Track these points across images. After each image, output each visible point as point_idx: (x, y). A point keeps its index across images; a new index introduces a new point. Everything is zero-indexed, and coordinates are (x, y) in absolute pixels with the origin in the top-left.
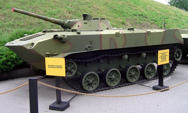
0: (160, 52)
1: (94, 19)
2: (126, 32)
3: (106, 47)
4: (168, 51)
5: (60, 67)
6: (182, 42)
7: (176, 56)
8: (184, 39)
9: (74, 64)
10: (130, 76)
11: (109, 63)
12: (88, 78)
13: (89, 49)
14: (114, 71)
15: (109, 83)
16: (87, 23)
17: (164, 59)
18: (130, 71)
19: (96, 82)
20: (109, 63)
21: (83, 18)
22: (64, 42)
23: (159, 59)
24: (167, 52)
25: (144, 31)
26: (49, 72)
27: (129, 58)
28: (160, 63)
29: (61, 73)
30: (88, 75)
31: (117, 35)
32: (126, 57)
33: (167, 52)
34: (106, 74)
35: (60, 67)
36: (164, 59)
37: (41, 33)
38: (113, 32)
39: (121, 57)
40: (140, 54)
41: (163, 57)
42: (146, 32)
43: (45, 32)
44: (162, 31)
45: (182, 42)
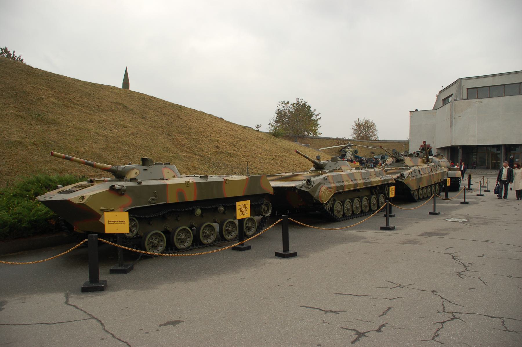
0: (238, 204)
1: (156, 164)
2: (197, 180)
3: (172, 199)
4: (248, 202)
5: (122, 222)
6: (272, 192)
7: (264, 210)
8: (275, 188)
9: (135, 221)
10: (205, 236)
11: (177, 220)
12: (152, 239)
13: (153, 202)
14: (185, 229)
15: (178, 245)
16: (389, 308)
17: (244, 212)
18: (203, 229)
19: (161, 243)
20: (177, 220)
21: (141, 162)
22: (123, 194)
23: (238, 212)
24: (247, 203)
25: (220, 179)
26: (109, 229)
27: (202, 213)
28: (239, 217)
29: (124, 228)
30: (152, 235)
31: (187, 184)
32: (199, 211)
33: (247, 203)
34: (174, 233)
35: (122, 222)
36: (244, 212)
37: (84, 183)
38: (181, 180)
39: (193, 212)
40: (216, 209)
41: (243, 210)
42: (223, 180)
43: (92, 182)
44: (244, 178)
45: (272, 192)
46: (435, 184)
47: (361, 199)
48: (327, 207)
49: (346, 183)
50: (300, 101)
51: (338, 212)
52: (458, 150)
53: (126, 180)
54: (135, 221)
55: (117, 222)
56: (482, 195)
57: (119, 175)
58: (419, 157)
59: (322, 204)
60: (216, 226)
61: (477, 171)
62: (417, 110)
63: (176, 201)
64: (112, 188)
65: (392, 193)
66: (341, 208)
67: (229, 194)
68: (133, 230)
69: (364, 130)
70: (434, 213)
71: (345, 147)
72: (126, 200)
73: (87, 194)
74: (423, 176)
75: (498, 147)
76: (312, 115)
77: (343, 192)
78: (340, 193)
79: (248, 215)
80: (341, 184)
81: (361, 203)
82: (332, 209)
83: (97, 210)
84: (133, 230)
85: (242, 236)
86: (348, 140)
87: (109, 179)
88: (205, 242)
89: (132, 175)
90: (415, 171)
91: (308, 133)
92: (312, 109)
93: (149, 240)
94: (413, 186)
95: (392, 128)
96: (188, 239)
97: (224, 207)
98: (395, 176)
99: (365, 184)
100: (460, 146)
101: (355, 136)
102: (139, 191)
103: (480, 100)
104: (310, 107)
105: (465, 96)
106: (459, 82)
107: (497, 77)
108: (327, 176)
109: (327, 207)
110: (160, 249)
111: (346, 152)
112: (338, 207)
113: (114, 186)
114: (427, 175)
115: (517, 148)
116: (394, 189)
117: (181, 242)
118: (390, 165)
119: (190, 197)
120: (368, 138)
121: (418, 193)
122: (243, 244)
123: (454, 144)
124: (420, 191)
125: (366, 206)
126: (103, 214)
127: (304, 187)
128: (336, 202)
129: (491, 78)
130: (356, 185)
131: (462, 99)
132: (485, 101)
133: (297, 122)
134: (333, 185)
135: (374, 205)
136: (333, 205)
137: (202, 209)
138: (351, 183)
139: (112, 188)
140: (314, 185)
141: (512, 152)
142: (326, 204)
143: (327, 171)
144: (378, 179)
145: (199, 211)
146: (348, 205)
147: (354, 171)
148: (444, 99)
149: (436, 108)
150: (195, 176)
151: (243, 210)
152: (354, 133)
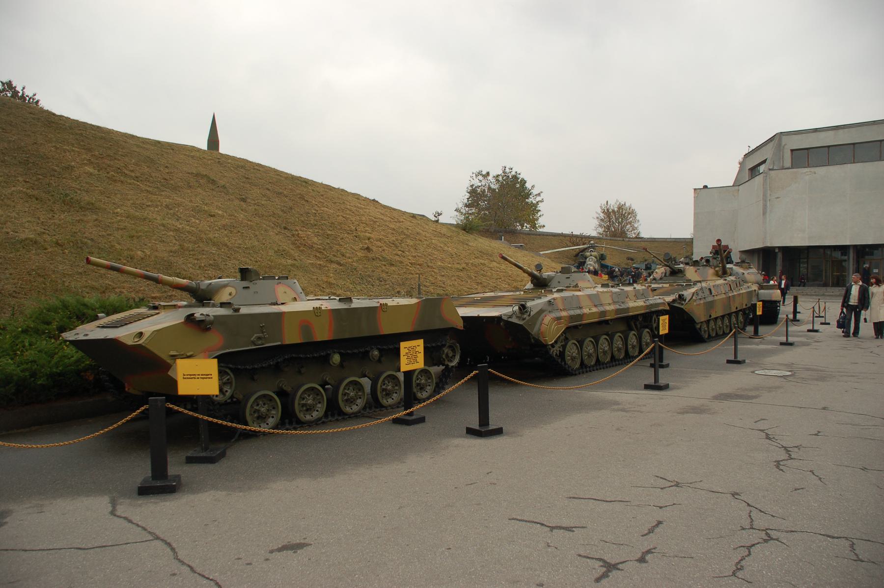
0: (403, 345)
1: (264, 278)
2: (334, 305)
3: (292, 336)
4: (421, 342)
5: (207, 376)
6: (460, 325)
7: (447, 355)
8: (465, 319)
9: (228, 374)
10: (347, 400)
11: (300, 372)
12: (258, 405)
13: (260, 342)
14: (313, 389)
15: (301, 416)
16: (660, 523)
17: (413, 359)
18: (345, 389)
19: (273, 412)
20: (300, 372)
21: (239, 275)
22: (208, 329)
23: (403, 360)
24: (419, 344)
25: (373, 303)
26: (185, 388)
27: (342, 361)
28: (404, 367)
29: (210, 387)
30: (257, 398)
31: (317, 311)
32: (336, 358)
33: (419, 344)
34: (295, 395)
35: (207, 376)
36: (413, 359)
37: (143, 310)
38: (306, 305)
39: (326, 359)
40: (366, 353)
41: (412, 356)
42: (378, 305)
43: (155, 308)
44: (414, 301)
45: (460, 325)
46: (737, 313)
47: (611, 337)
48: (555, 351)
49: (586, 311)
50: (507, 170)
51: (573, 359)
52: (775, 254)
53: (214, 306)
54: (228, 374)
55: (198, 376)
56: (817, 331)
57: (202, 297)
58: (710, 266)
59: (545, 346)
60: (366, 382)
61: (807, 290)
62: (705, 187)
63: (298, 341)
64: (190, 318)
65: (664, 326)
66: (578, 353)
67: (387, 328)
68: (225, 389)
69: (617, 220)
70: (736, 362)
71: (584, 250)
72: (214, 339)
73: (147, 329)
74: (716, 298)
75: (844, 249)
76: (528, 195)
77: (580, 325)
78: (576, 327)
79: (420, 364)
80: (578, 312)
81: (611, 344)
82: (562, 354)
83: (163, 356)
84: (225, 389)
85: (410, 400)
86: (589, 238)
87: (185, 303)
88: (348, 410)
89: (224, 296)
90: (703, 289)
91: (522, 226)
92: (528, 185)
93: (252, 406)
94: (699, 315)
95: (664, 217)
96: (319, 405)
97: (380, 350)
98: (669, 299)
99: (617, 311)
100: (779, 247)
101: (601, 230)
102: (235, 323)
103: (813, 169)
104: (525, 182)
105: (788, 163)
106: (778, 138)
107: (841, 131)
108: (554, 299)
109: (555, 351)
110: (271, 421)
111: (586, 258)
112: (572, 350)
113: (193, 315)
114: (724, 296)
115: (875, 252)
116: (667, 321)
117: (307, 410)
118: (661, 279)
119: (322, 334)
120: (623, 234)
121: (708, 327)
122: (411, 414)
123: (769, 245)
124: (712, 324)
125: (619, 350)
126: (175, 362)
127: (514, 316)
128: (570, 343)
129: (831, 133)
130: (604, 313)
131: (783, 168)
132: (821, 171)
133: (502, 206)
134: (564, 314)
135: (633, 347)
136: (564, 347)
137: (341, 355)
138: (594, 310)
139: (190, 318)
140: (532, 313)
141: (867, 257)
142: (553, 346)
143: (554, 290)
144: (640, 303)
145: (336, 358)
146: (589, 348)
147: (600, 289)
148: (752, 168)
149: (738, 183)
150: (329, 299)
151: (412, 356)
152: (600, 226)
